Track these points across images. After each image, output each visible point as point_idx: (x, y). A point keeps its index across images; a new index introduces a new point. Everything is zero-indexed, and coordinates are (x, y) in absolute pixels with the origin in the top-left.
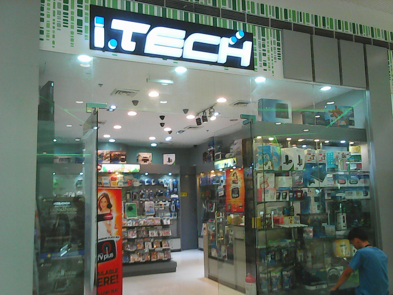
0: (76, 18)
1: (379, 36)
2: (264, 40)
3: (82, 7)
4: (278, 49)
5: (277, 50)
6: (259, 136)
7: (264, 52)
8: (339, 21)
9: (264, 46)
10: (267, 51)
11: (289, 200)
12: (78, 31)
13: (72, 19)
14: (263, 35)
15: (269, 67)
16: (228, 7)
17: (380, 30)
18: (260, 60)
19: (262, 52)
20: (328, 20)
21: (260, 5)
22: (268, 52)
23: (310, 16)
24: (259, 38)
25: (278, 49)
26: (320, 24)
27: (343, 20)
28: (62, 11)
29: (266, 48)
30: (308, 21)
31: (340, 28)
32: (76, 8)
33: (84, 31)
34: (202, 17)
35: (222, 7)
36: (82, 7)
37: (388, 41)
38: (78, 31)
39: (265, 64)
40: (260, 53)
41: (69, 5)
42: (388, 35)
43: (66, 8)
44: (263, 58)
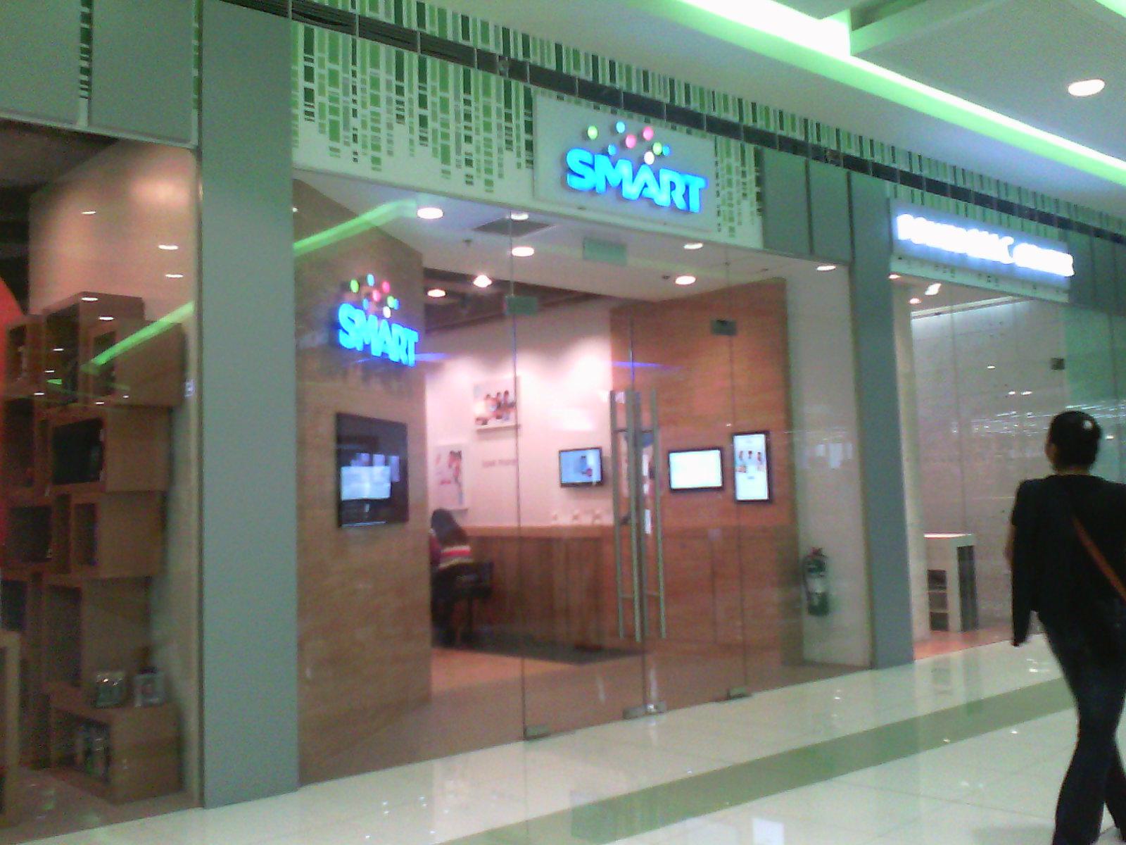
0: (417, 111)
1: (793, 129)
2: (467, 102)
3: (312, 61)
4: (398, 102)
5: (395, 105)
6: (1013, 391)
7: (468, 133)
8: (781, 113)
9: (468, 117)
10: (473, 129)
11: (723, 482)
12: (307, 113)
13: (411, 114)
14: (467, 90)
15: (478, 170)
16: (384, 15)
17: (427, 7)
18: (458, 151)
19: (463, 132)
20: (588, 59)
21: (436, 10)
22: (364, 105)
23: (491, 28)
24: (457, 97)
25: (398, 102)
26: (475, 35)
27: (788, 112)
28: (394, 97)
29: (473, 124)
30: (726, 109)
31: (782, 128)
32: (416, 92)
33: (316, 115)
34: (476, 76)
35: (480, 45)
36: (312, 61)
37: (470, 43)
38: (307, 113)
39: (469, 163)
40: (458, 136)
41: (405, 84)
42: (604, 70)
43: (400, 91)
44: (466, 147)
